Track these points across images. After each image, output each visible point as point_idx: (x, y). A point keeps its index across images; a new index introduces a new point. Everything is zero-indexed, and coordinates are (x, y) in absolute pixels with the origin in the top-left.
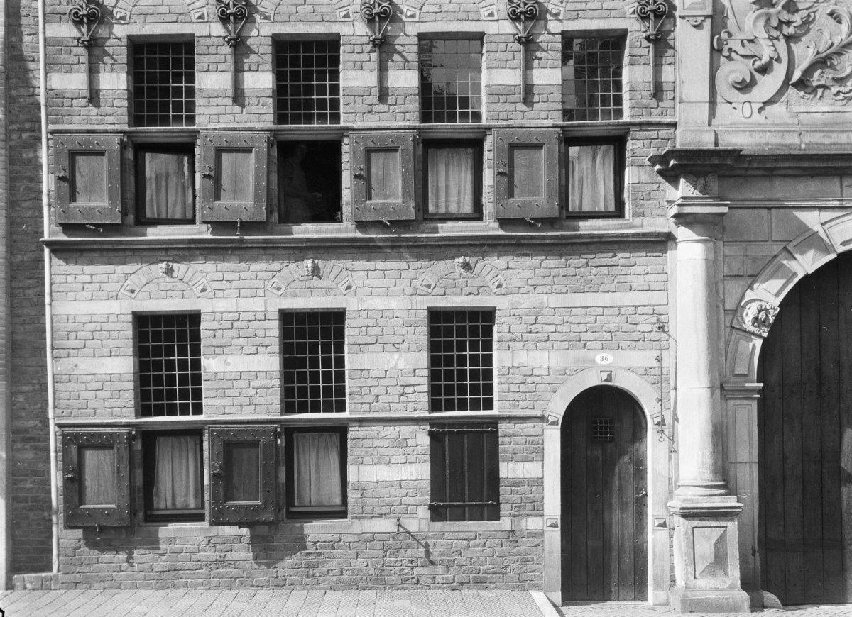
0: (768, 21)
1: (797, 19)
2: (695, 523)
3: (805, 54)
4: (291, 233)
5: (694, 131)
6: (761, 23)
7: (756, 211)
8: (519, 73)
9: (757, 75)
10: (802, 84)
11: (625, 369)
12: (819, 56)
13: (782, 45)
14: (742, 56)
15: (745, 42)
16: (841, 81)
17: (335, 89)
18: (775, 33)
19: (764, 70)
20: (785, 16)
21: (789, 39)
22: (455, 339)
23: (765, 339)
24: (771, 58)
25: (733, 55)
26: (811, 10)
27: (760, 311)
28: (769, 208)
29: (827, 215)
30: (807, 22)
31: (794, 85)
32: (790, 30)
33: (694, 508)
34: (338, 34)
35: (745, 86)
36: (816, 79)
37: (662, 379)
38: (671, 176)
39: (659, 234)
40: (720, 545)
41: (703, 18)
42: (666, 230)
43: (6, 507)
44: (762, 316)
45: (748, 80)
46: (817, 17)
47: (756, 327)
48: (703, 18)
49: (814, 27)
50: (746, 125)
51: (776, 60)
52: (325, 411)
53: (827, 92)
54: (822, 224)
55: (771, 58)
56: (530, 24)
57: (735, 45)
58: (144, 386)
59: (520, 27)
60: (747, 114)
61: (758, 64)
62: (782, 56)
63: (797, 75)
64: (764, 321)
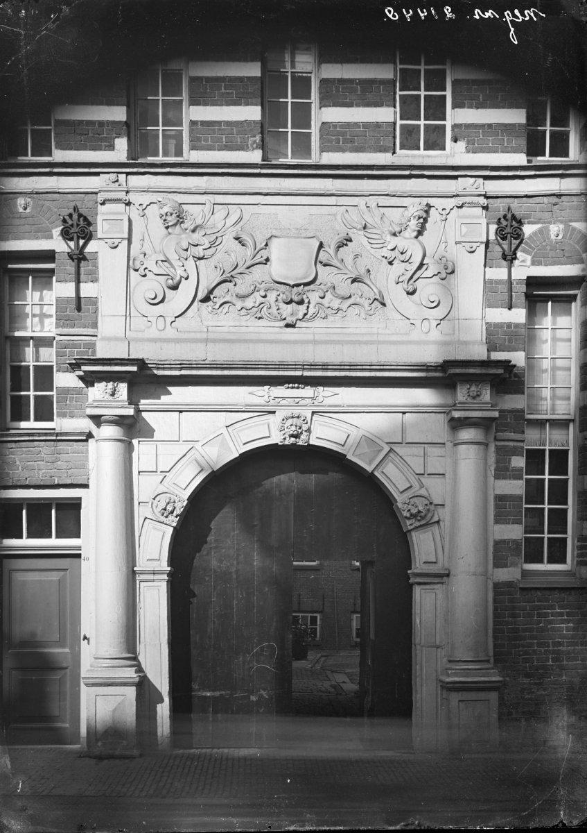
3: (209, 276)
8: (72, 285)
9: (168, 292)
13: (191, 264)
15: (160, 262)
18: (184, 254)
22: (546, 506)
23: (175, 528)
24: (181, 277)
26: (218, 235)
28: (181, 412)
32: (199, 251)
34: (54, 251)
41: (120, 240)
43: (169, 647)
48: (120, 240)
52: (550, 561)
55: (181, 277)
58: (563, 538)
59: (72, 244)
60: (425, 330)
61: (170, 282)
63: (201, 295)
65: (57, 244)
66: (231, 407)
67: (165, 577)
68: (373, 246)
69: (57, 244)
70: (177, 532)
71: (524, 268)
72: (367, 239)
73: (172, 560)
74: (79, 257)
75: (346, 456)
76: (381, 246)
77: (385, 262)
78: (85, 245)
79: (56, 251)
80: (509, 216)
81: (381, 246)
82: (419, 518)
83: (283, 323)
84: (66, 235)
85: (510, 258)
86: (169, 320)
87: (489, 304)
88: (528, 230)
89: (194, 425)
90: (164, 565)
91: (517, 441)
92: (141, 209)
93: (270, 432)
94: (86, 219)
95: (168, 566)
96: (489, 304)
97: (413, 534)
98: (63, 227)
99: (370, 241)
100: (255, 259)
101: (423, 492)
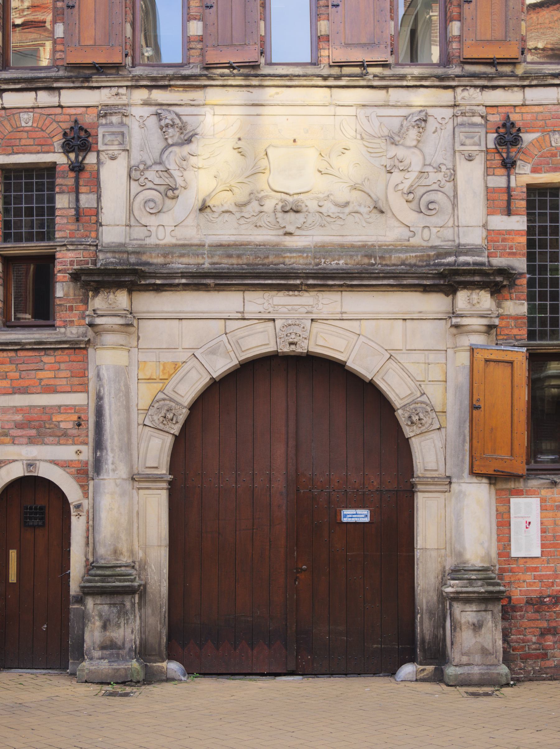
59: (72, 156)
65: (60, 158)
66: (193, 315)
67: (165, 485)
68: (372, 155)
69: (60, 158)
70: (178, 440)
71: (525, 176)
72: (366, 148)
73: (172, 469)
74: (77, 168)
75: (346, 362)
76: (381, 154)
77: (384, 171)
78: (84, 158)
79: (57, 163)
80: (76, 128)
81: (381, 154)
82: (420, 426)
83: (281, 232)
84: (67, 148)
85: (509, 165)
86: (168, 229)
87: (491, 211)
88: (527, 138)
89: (190, 334)
90: (164, 470)
91: (370, 339)
92: (141, 121)
93: (259, 342)
94: (86, 131)
95: (170, 474)
96: (491, 211)
97: (413, 439)
98: (64, 140)
99: (370, 150)
100: (255, 168)
101: (424, 398)
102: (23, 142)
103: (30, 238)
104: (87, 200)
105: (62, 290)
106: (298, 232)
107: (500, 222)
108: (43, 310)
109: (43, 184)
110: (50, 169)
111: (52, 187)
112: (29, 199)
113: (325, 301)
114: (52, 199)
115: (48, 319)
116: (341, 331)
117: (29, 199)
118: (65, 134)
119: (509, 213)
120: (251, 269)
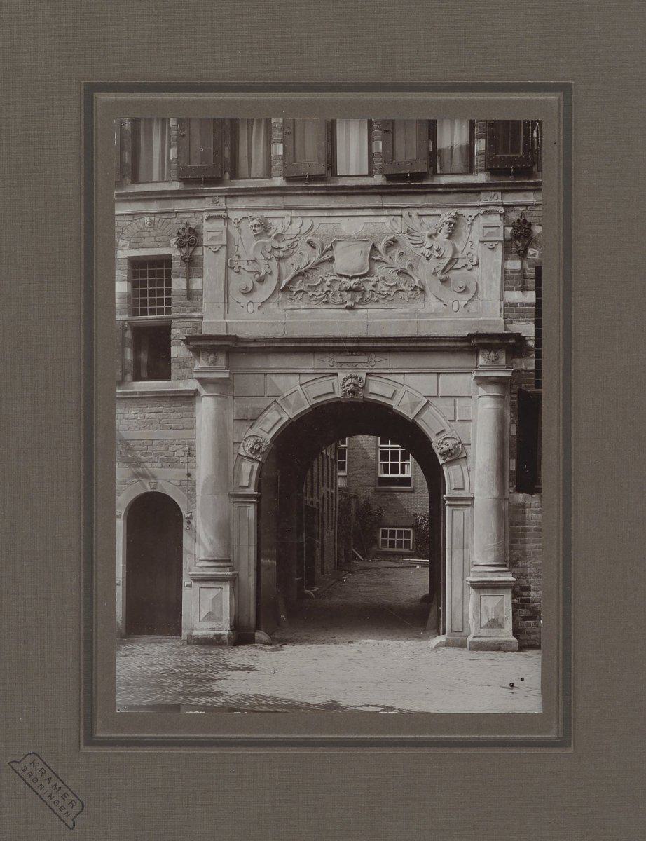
0: (264, 248)
1: (284, 245)
2: (204, 585)
4: (133, 388)
5: (213, 322)
6: (260, 248)
7: (256, 375)
10: (286, 289)
11: (167, 482)
12: (299, 271)
13: (274, 263)
14: (248, 271)
16: (314, 288)
17: (169, 292)
18: (269, 256)
19: (261, 281)
20: (276, 245)
21: (279, 259)
25: (242, 270)
27: (256, 443)
28: (266, 374)
29: (304, 379)
30: (291, 247)
31: (282, 290)
33: (198, 575)
35: (248, 292)
36: (298, 286)
37: (189, 486)
38: (197, 351)
39: (191, 391)
40: (217, 599)
42: (194, 389)
44: (257, 447)
45: (250, 288)
46: (299, 244)
47: (253, 454)
49: (297, 251)
50: (253, 319)
51: (270, 274)
53: (305, 296)
54: (301, 385)
56: (191, 249)
57: (245, 265)
60: (251, 311)
62: (274, 272)
64: (259, 450)
68: (415, 246)
69: (176, 253)
87: (506, 287)
90: (252, 491)
102: (147, 239)
103: (152, 312)
104: (197, 284)
105: (177, 351)
106: (357, 306)
107: (515, 296)
108: (159, 366)
109: (154, 271)
110: (166, 261)
111: (169, 273)
112: (152, 283)
113: (377, 359)
114: (169, 283)
115: (530, 174)
116: (391, 382)
117: (152, 283)
118: (179, 233)
119: (524, 289)
120: (558, 724)
